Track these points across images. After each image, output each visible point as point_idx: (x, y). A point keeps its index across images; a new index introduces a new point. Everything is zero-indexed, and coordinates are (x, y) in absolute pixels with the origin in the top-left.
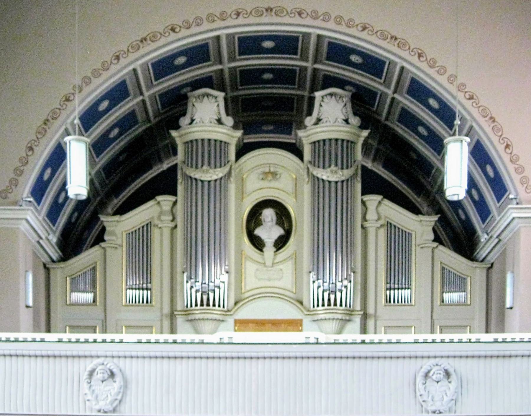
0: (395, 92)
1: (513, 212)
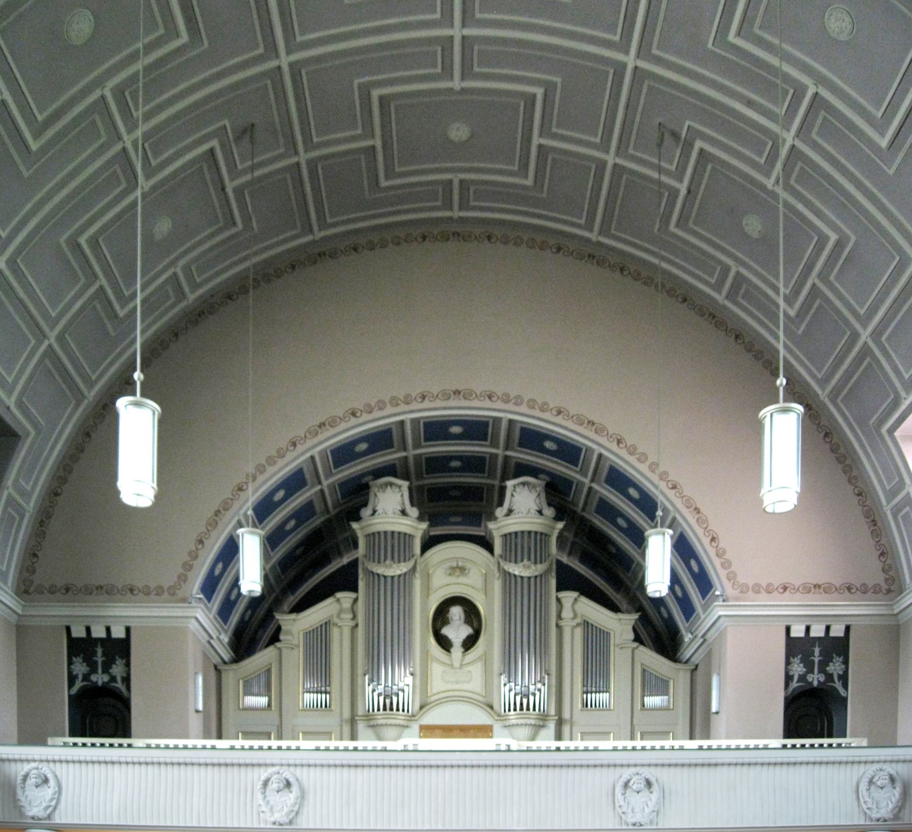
0: (592, 481)
1: (719, 610)
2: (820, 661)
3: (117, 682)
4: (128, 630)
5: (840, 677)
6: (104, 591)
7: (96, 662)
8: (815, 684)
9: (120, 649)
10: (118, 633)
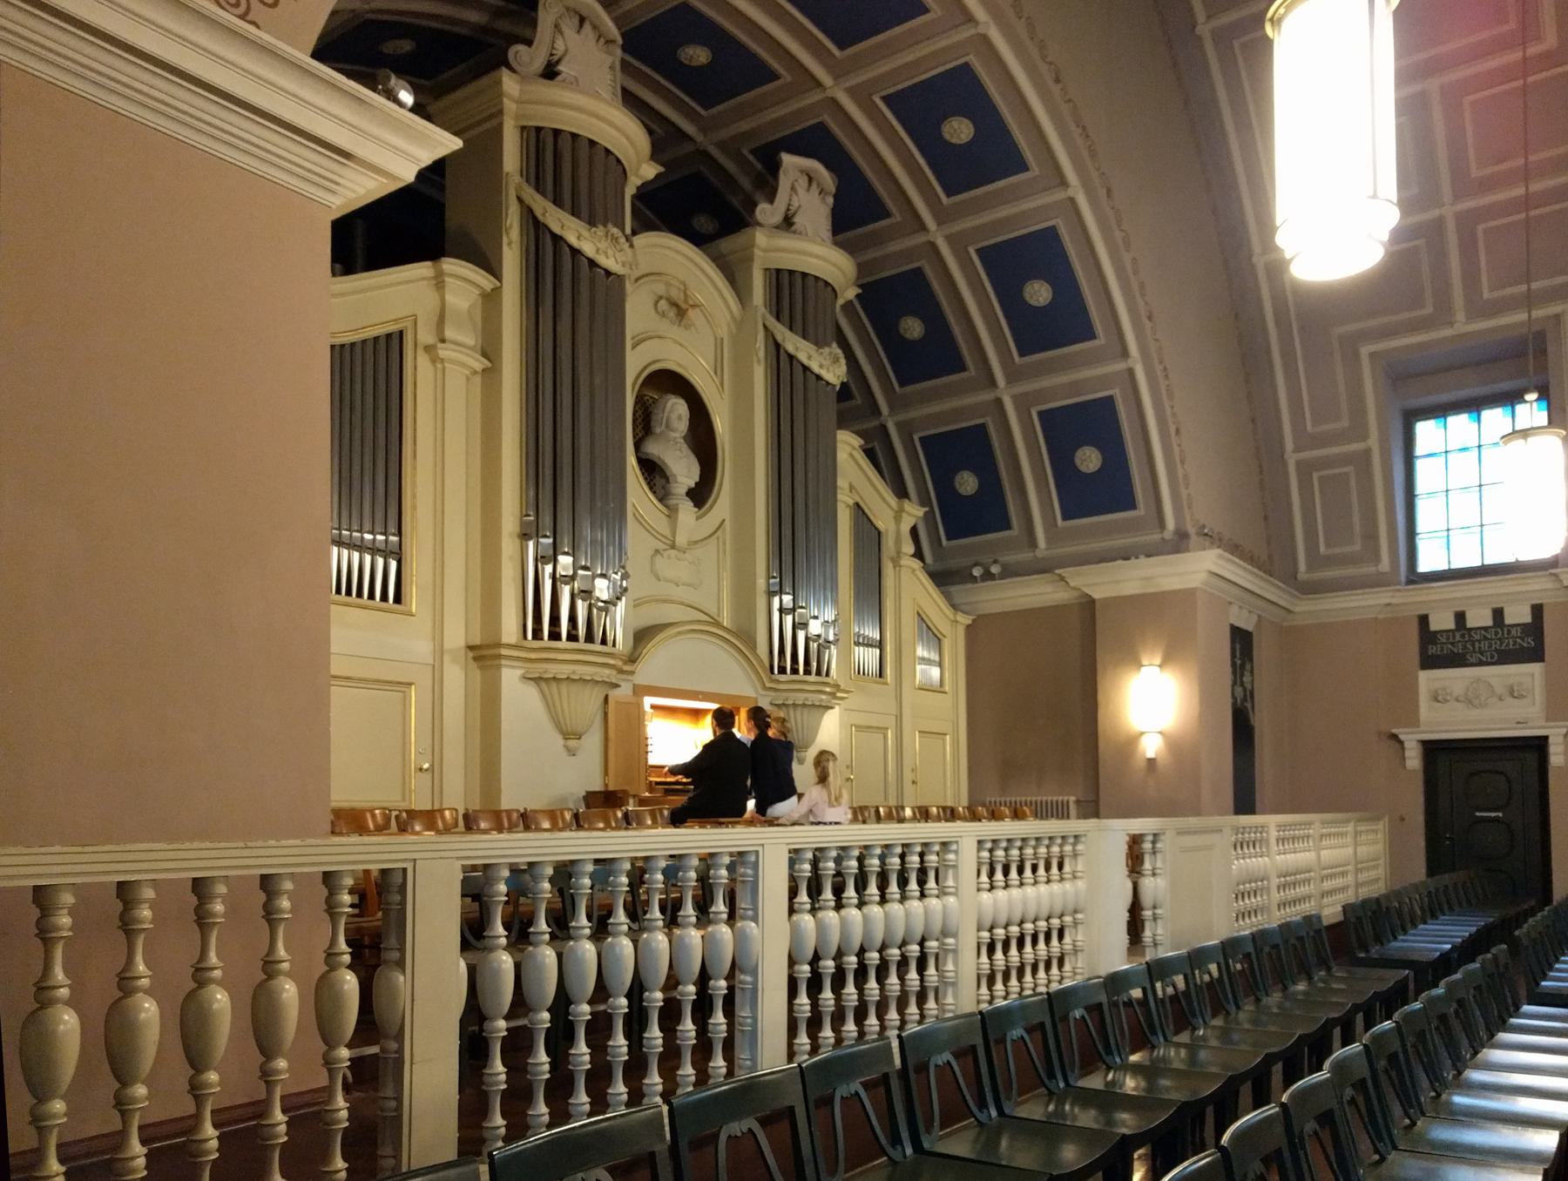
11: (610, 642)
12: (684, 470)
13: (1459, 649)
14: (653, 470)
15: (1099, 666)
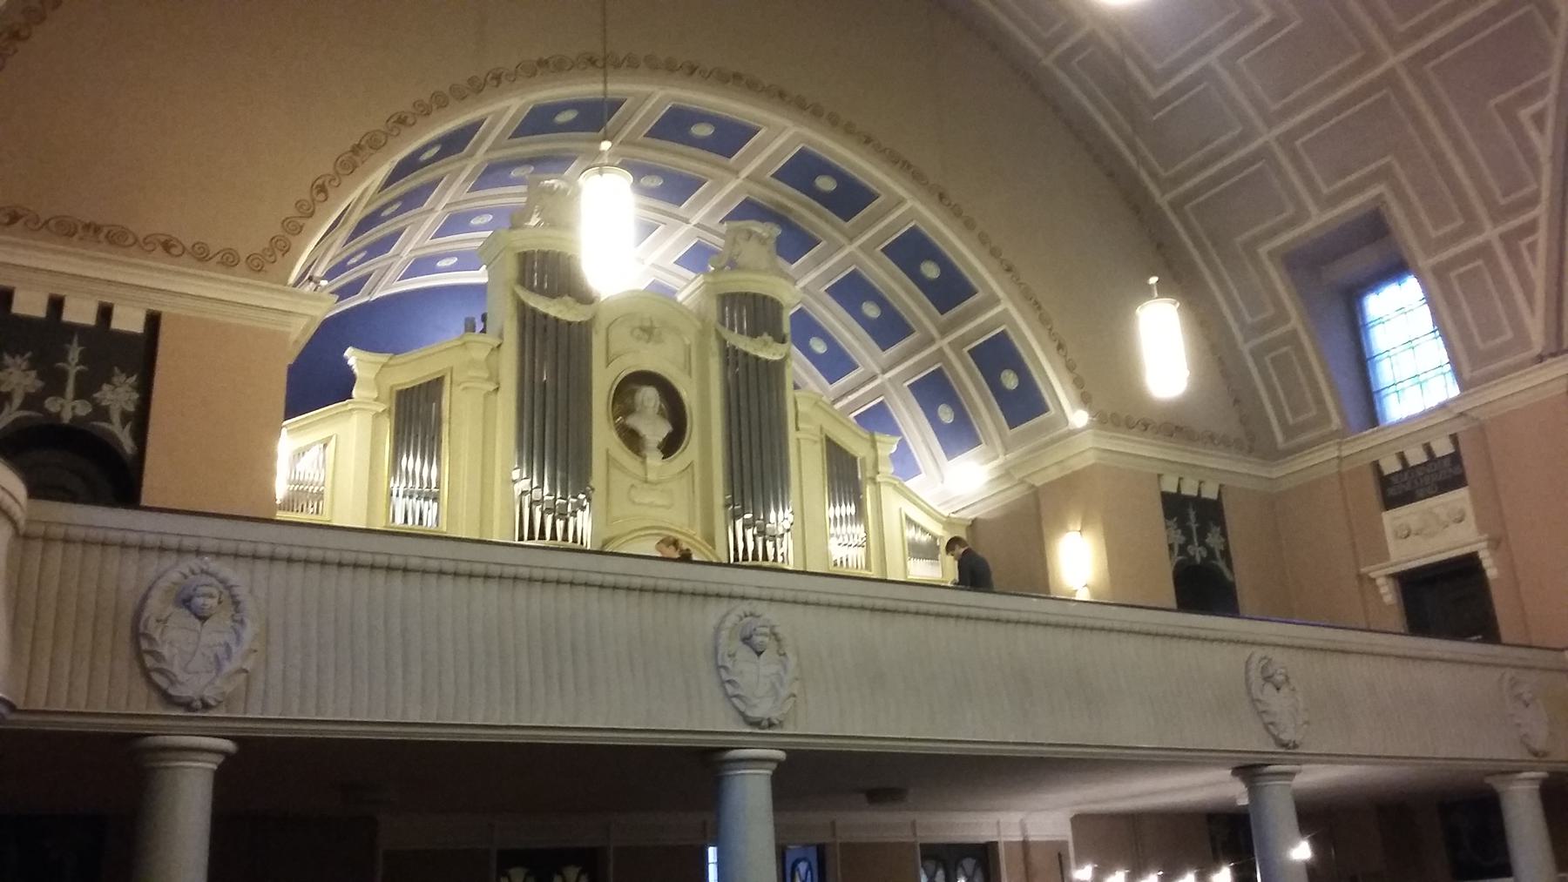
2: (79, 375)
3: (108, 420)
4: (153, 320)
5: (125, 417)
6: (102, 236)
7: (63, 375)
8: (1198, 559)
9: (139, 354)
10: (128, 320)
11: (771, 557)
12: (654, 430)
13: (1408, 487)
14: (632, 439)
15: (1045, 530)
